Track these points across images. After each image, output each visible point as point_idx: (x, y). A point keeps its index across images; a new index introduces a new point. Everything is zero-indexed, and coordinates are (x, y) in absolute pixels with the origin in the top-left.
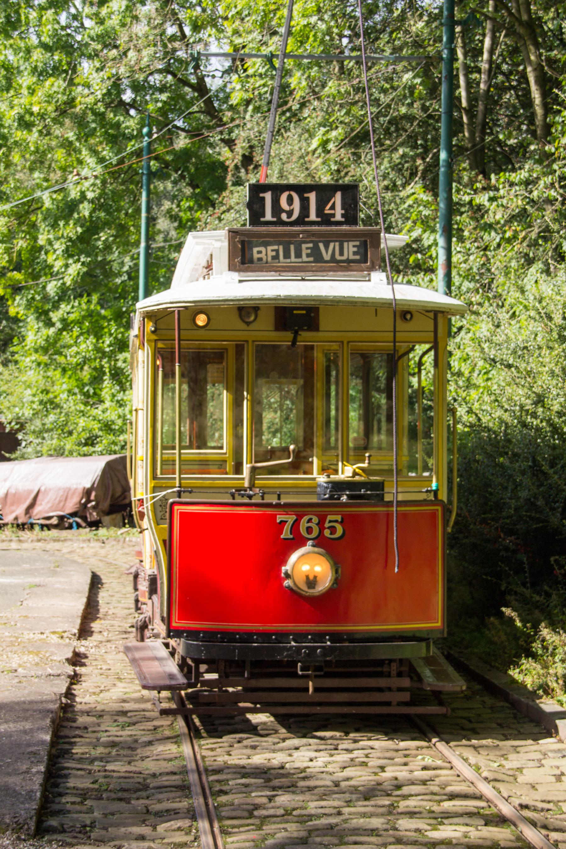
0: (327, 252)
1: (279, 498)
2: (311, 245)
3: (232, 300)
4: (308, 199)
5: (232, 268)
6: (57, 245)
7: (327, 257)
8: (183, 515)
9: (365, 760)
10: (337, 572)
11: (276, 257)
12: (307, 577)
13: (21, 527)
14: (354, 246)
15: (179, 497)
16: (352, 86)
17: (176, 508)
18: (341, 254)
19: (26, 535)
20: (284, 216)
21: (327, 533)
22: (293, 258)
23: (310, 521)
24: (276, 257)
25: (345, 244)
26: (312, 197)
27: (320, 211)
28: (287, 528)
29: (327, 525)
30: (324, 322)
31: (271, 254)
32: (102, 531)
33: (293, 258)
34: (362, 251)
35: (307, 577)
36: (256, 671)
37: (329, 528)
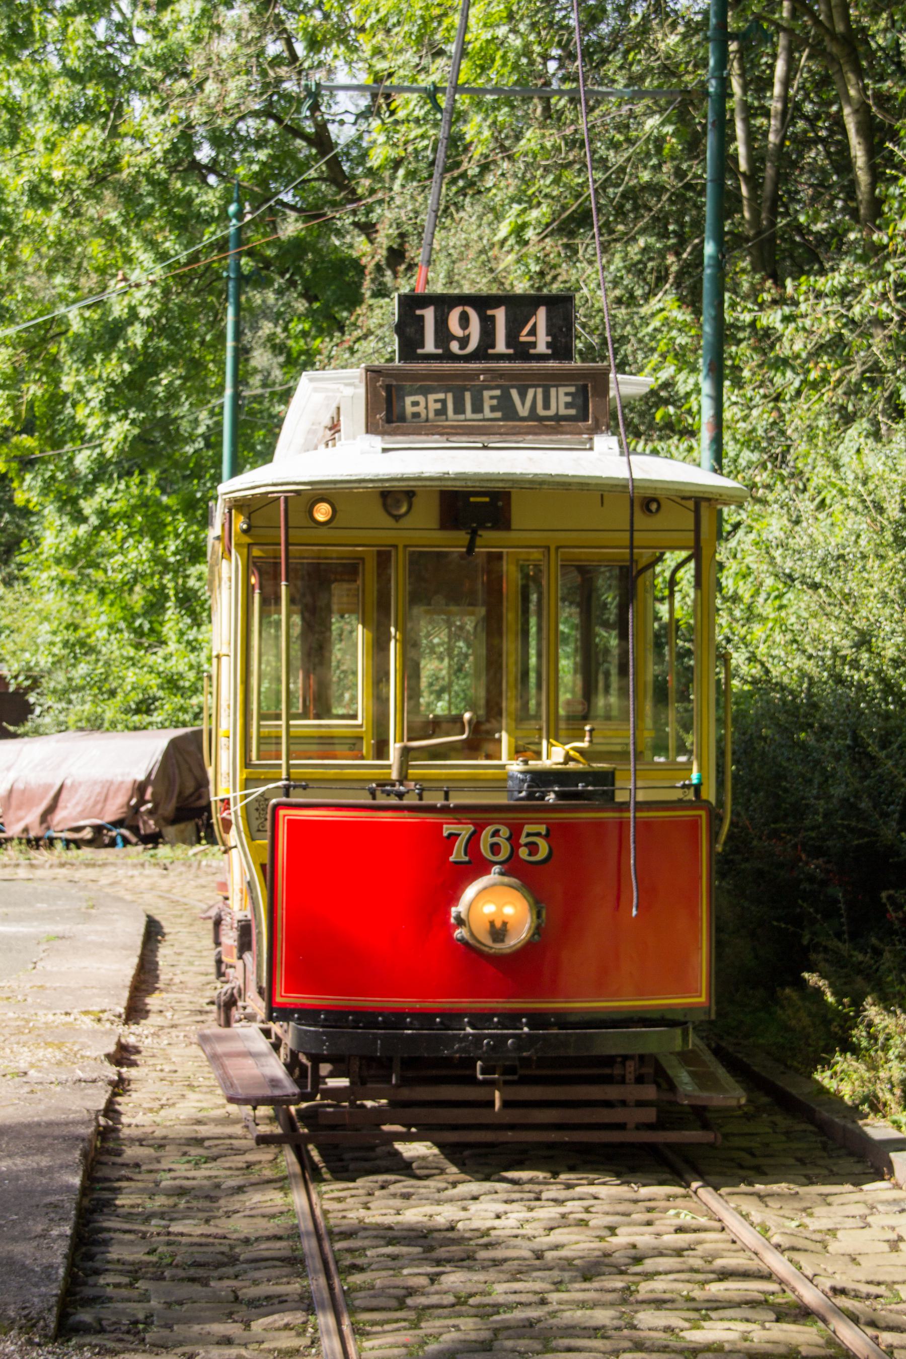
0: (523, 404)
1: (447, 798)
2: (497, 392)
3: (371, 481)
4: (493, 318)
5: (371, 428)
6: (91, 393)
7: (523, 411)
8: (293, 824)
9: (585, 1216)
10: (539, 916)
11: (441, 412)
12: (492, 924)
13: (34, 843)
14: (567, 394)
15: (287, 795)
16: (564, 138)
17: (282, 812)
18: (547, 406)
19: (42, 856)
20: (455, 347)
21: (523, 853)
22: (469, 414)
23: (496, 833)
24: (441, 412)
25: (553, 391)
26: (500, 315)
27: (512, 338)
28: (459, 846)
29: (523, 840)
30: (518, 516)
31: (434, 406)
32: (164, 851)
33: (469, 414)
34: (580, 401)
35: (492, 924)
36: (410, 1074)
37: (526, 845)
